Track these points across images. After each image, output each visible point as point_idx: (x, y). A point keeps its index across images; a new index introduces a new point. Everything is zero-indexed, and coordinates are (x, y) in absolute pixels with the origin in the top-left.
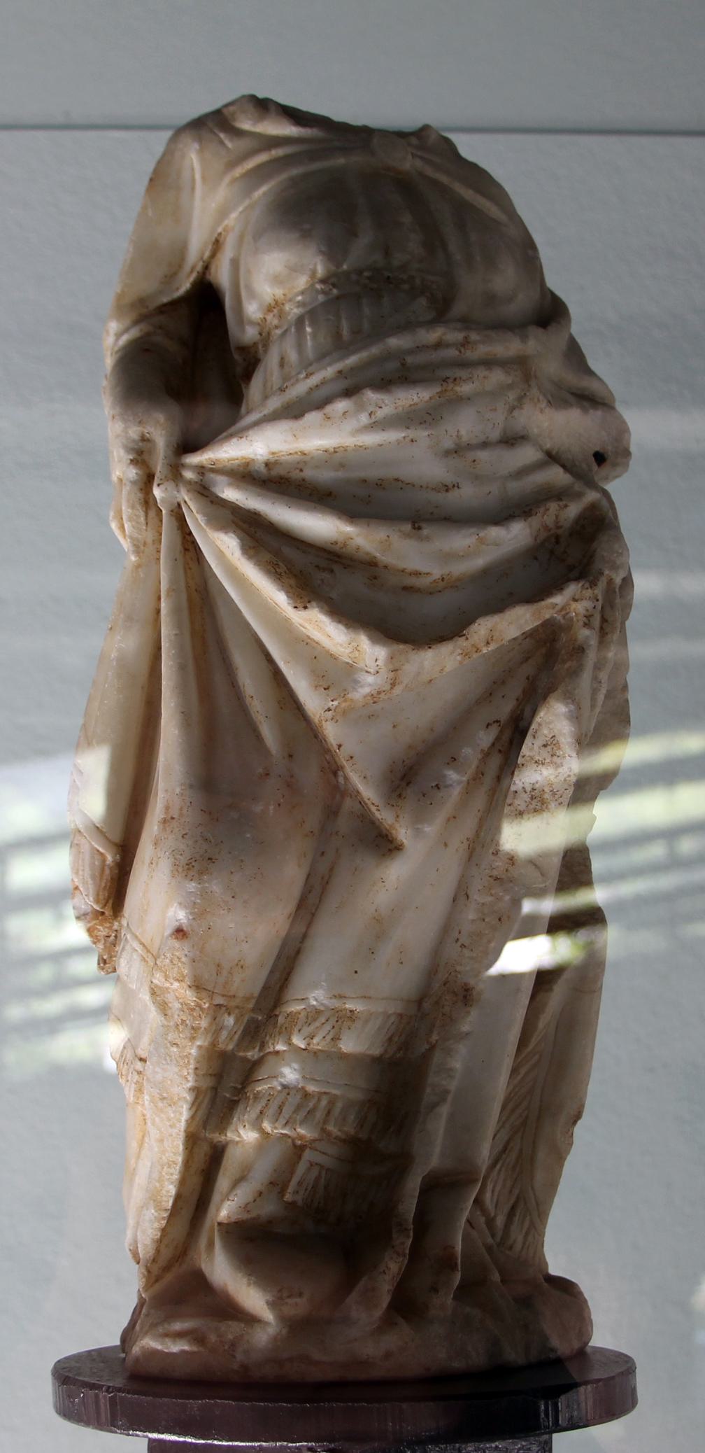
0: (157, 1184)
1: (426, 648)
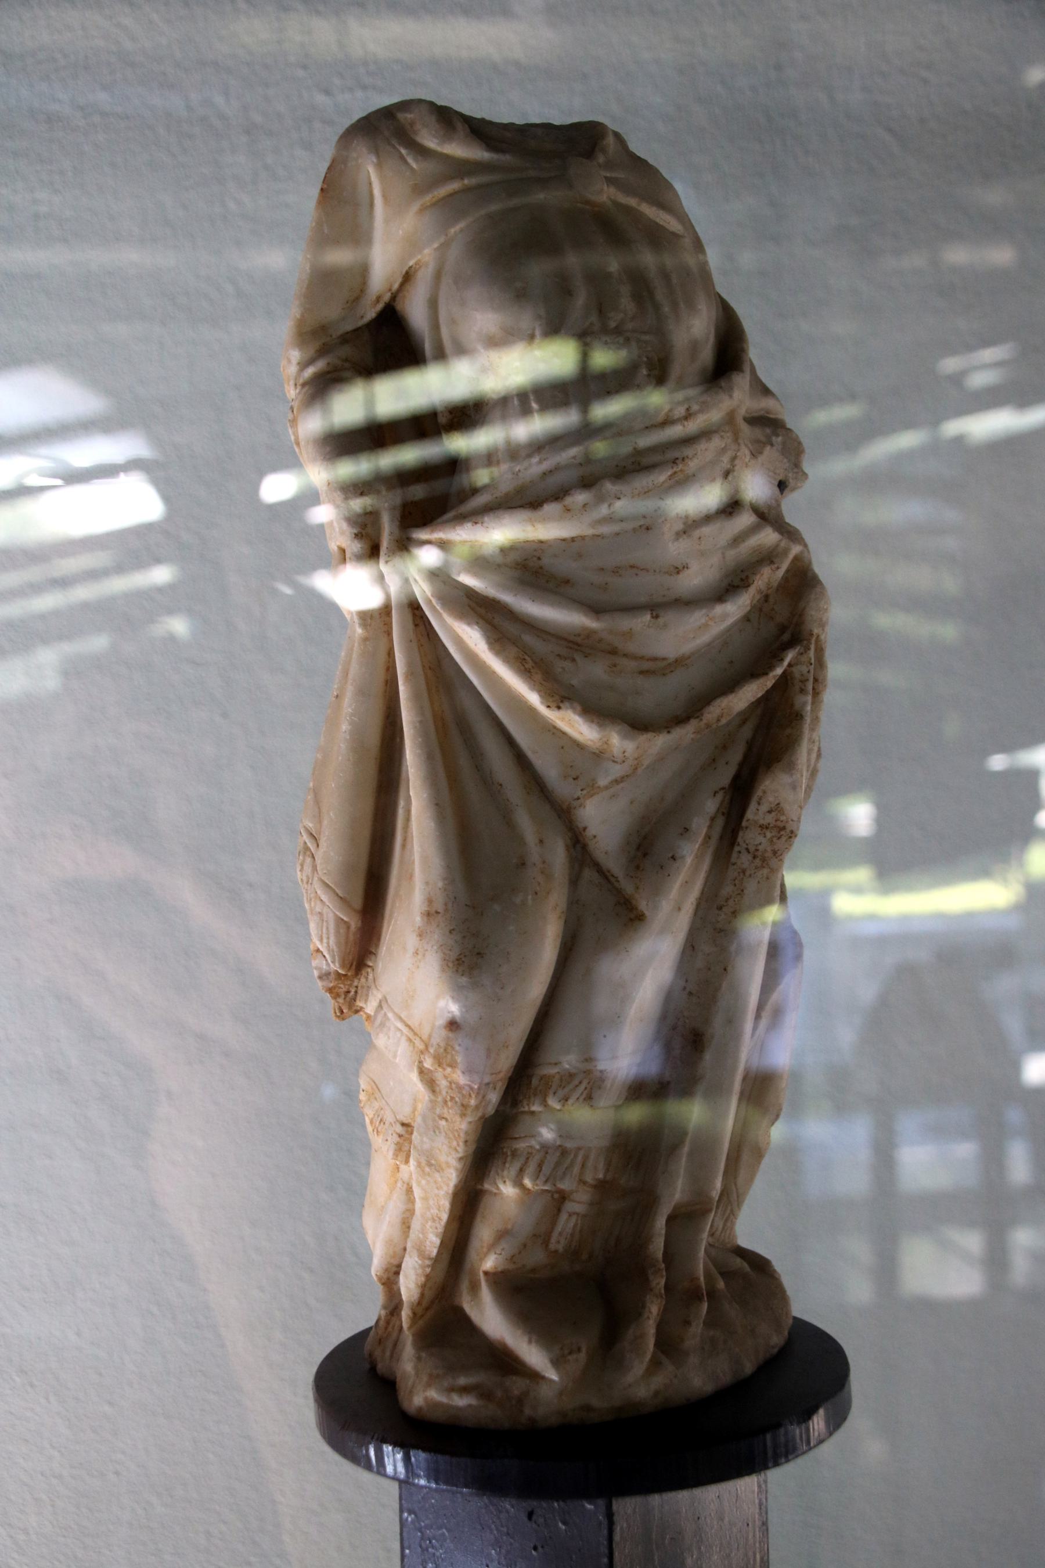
0: (421, 1236)
1: (666, 732)
